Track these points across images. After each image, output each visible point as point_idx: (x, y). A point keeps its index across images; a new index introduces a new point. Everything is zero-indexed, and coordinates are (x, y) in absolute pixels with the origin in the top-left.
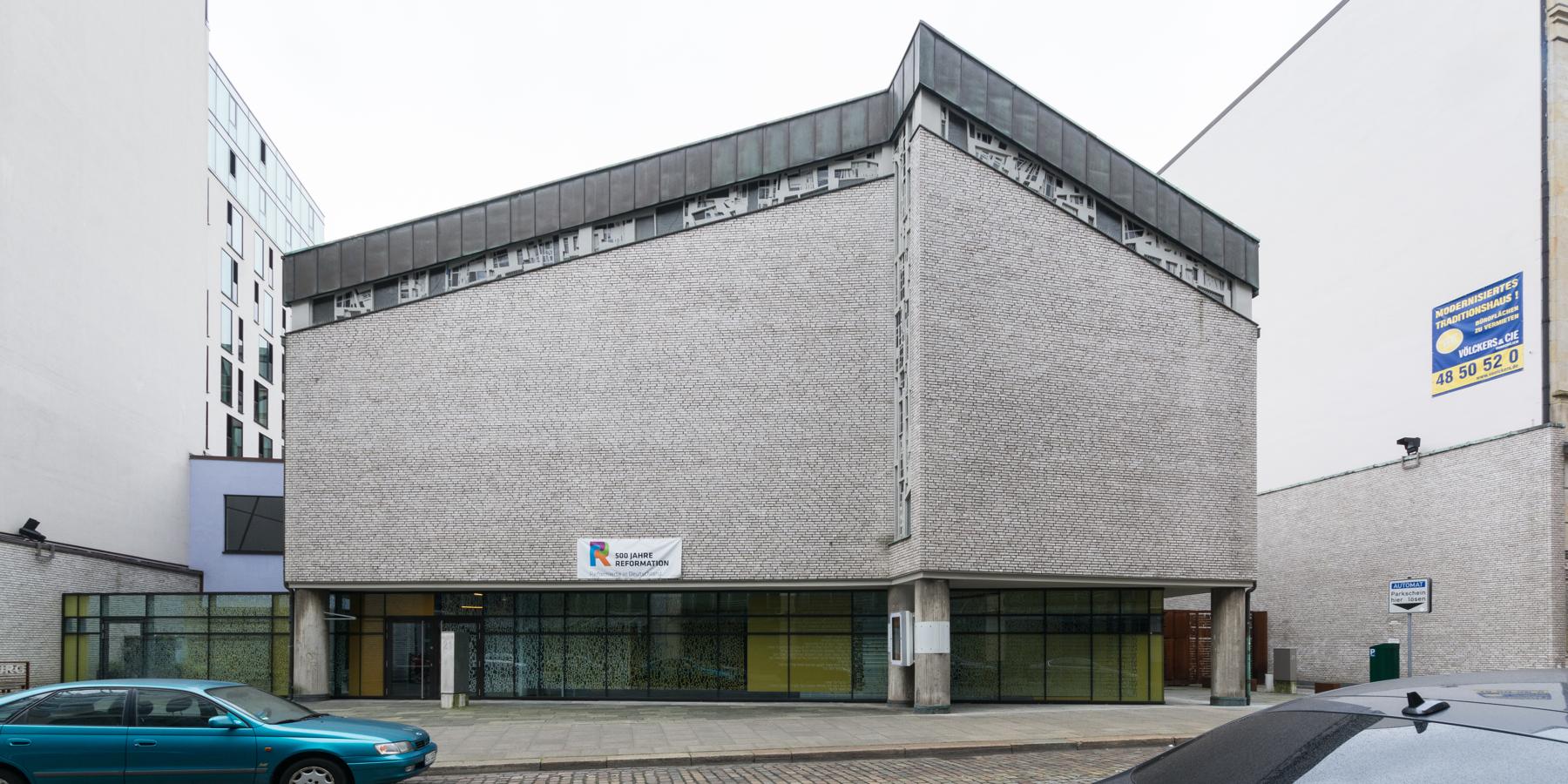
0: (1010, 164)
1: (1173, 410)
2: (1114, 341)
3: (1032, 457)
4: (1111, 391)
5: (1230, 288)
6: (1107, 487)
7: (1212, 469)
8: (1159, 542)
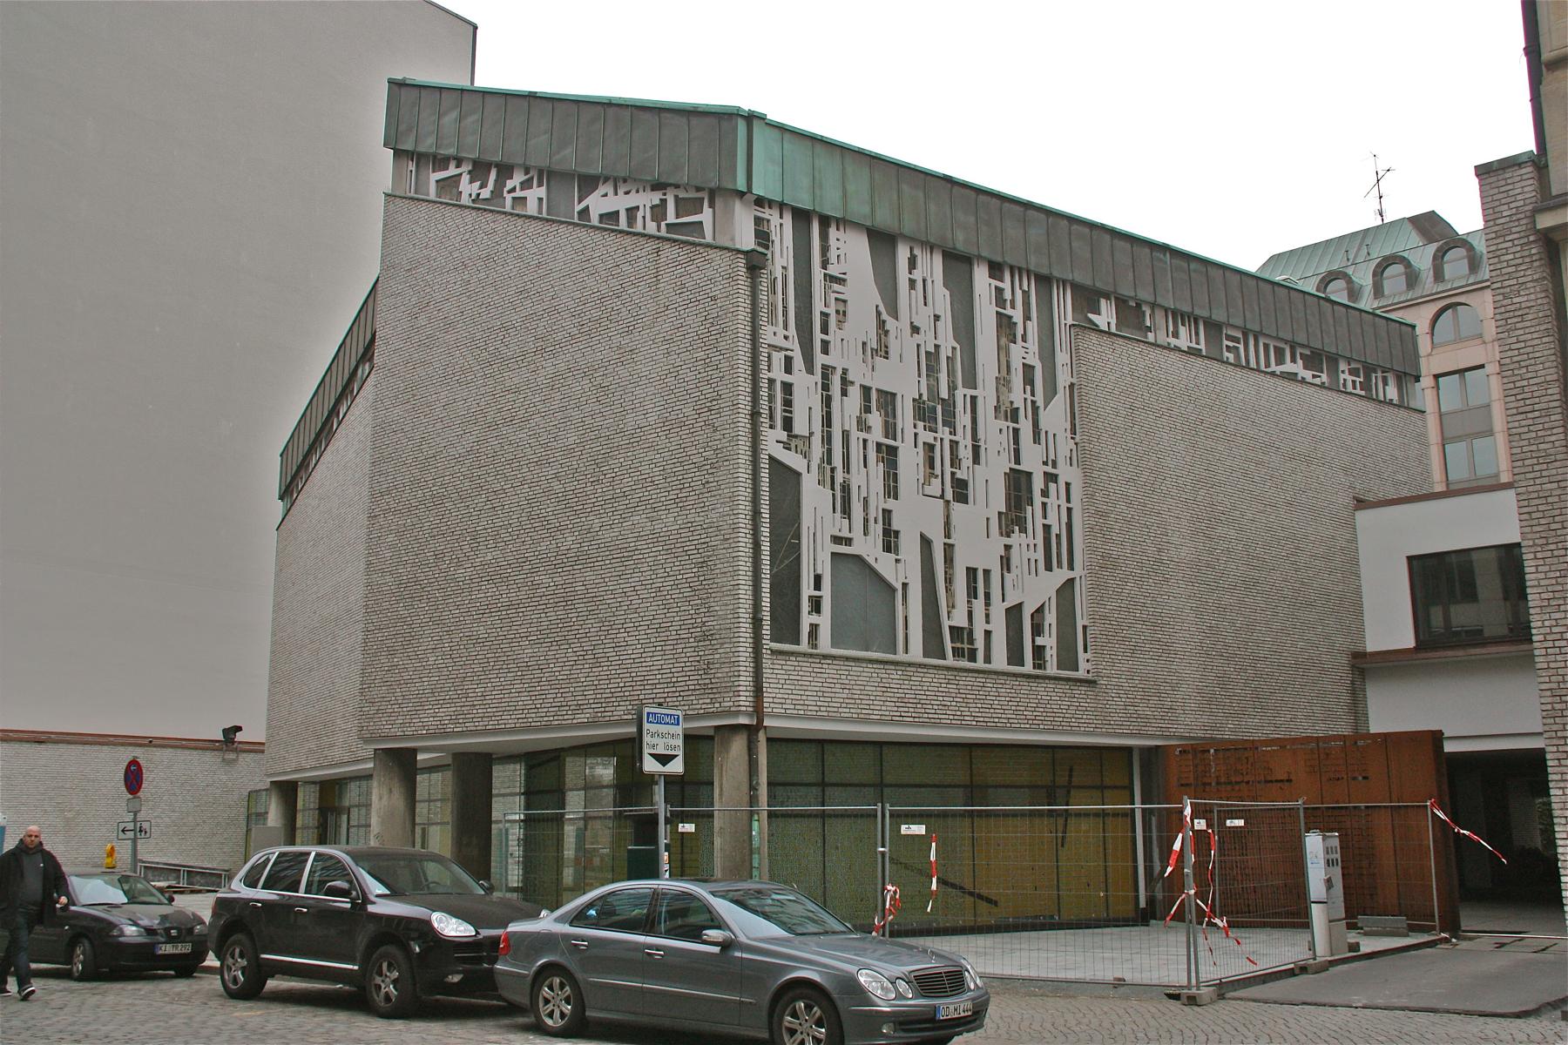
3: (459, 565)
7: (670, 521)
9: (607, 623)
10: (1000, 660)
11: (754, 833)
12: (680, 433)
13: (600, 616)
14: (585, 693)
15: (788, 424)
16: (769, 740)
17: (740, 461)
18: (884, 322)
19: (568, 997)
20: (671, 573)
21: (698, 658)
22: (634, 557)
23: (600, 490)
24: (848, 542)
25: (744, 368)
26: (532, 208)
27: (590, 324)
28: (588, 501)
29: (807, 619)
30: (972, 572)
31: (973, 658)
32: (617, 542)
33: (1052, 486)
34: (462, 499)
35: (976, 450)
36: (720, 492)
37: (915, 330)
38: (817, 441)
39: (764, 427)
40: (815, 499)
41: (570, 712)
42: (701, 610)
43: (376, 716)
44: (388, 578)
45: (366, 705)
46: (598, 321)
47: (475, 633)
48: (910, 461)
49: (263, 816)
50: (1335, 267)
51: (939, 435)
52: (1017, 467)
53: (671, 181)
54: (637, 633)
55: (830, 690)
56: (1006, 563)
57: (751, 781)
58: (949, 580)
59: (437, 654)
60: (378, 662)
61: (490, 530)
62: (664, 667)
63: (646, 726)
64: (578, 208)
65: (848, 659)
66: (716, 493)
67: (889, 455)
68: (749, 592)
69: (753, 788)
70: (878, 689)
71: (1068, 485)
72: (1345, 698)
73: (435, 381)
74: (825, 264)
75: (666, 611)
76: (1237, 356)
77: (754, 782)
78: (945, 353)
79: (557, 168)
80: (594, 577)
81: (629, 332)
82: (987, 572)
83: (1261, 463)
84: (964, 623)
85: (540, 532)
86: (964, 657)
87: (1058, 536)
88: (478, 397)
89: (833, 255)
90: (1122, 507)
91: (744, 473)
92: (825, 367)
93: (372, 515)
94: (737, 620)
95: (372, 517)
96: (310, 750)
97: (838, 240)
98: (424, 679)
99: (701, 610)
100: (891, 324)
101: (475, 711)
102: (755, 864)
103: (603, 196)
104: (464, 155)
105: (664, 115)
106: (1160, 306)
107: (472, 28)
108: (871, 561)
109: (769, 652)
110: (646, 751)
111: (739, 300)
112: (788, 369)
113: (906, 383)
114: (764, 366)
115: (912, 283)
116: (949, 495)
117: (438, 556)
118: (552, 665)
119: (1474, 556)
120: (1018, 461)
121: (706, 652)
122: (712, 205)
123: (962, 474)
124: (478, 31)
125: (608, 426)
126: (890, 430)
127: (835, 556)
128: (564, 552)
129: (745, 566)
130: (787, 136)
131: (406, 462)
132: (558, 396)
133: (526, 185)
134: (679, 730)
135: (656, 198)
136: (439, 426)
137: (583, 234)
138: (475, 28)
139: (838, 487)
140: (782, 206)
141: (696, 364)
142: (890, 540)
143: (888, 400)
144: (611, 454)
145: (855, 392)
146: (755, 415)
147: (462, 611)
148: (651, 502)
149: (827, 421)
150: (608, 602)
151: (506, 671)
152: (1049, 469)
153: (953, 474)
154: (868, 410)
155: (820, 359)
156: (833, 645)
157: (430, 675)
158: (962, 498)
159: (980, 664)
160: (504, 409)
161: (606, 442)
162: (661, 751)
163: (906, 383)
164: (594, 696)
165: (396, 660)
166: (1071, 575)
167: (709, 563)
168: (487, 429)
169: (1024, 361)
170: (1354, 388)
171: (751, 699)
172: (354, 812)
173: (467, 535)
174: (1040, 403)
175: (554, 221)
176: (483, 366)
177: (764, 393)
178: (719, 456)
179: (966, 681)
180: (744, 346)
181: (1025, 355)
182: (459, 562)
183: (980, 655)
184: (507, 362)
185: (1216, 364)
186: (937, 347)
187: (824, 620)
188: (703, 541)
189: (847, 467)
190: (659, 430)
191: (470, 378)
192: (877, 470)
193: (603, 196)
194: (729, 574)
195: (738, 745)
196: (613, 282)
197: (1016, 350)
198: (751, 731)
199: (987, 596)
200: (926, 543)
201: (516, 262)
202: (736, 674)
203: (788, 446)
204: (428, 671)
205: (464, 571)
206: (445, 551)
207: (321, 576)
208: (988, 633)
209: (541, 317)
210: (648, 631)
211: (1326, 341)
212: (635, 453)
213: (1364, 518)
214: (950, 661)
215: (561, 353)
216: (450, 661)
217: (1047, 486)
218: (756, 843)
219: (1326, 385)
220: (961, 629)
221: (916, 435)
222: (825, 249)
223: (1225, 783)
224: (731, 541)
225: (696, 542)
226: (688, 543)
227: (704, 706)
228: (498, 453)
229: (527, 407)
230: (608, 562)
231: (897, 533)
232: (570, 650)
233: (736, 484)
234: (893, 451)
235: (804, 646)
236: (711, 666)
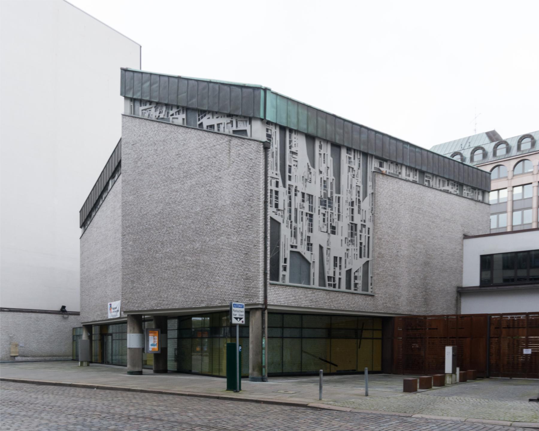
0: (154, 113)
1: (215, 210)
2: (188, 182)
3: (157, 252)
4: (187, 209)
5: (250, 123)
6: (185, 260)
7: (234, 239)
8: (208, 287)
9: (212, 274)
10: (343, 287)
11: (263, 343)
12: (239, 208)
13: (209, 271)
14: (204, 297)
15: (277, 206)
16: (268, 313)
17: (260, 218)
18: (310, 169)
20: (235, 257)
22: (222, 251)
23: (209, 228)
24: (296, 247)
25: (262, 185)
27: (204, 167)
28: (205, 231)
29: (282, 273)
31: (334, 286)
32: (216, 246)
33: (364, 229)
34: (157, 230)
35: (339, 216)
36: (253, 229)
39: (269, 207)
40: (285, 231)
41: (199, 303)
42: (246, 270)
43: (128, 304)
44: (130, 257)
45: (124, 300)
47: (163, 276)
48: (317, 219)
49: (80, 336)
50: (456, 150)
51: (327, 211)
52: (352, 222)
53: (235, 114)
54: (222, 277)
55: (288, 297)
56: (347, 255)
57: (262, 326)
59: (150, 283)
60: (128, 285)
61: (168, 241)
62: (233, 288)
63: (233, 308)
64: (198, 123)
65: (294, 287)
66: (251, 229)
68: (263, 264)
69: (263, 329)
70: (304, 297)
71: (369, 228)
72: (454, 302)
73: (145, 187)
74: (290, 147)
75: (233, 270)
77: (264, 327)
79: (190, 106)
80: (207, 258)
81: (219, 171)
82: (340, 258)
83: (433, 222)
85: (187, 242)
86: (331, 286)
87: (365, 246)
88: (162, 193)
89: (293, 144)
90: (386, 237)
91: (262, 223)
92: (289, 185)
93: (123, 234)
94: (259, 273)
95: (123, 235)
96: (98, 315)
97: (295, 138)
98: (145, 292)
99: (246, 270)
100: (312, 170)
102: (263, 353)
104: (153, 100)
105: (232, 87)
106: (404, 165)
108: (303, 254)
109: (269, 284)
110: (233, 316)
111: (261, 160)
112: (277, 186)
113: (316, 190)
114: (269, 185)
117: (149, 250)
118: (192, 287)
120: (353, 220)
121: (248, 284)
123: (334, 224)
124: (142, 48)
125: (212, 205)
126: (311, 208)
127: (291, 252)
128: (196, 249)
129: (262, 255)
130: (278, 97)
131: (136, 216)
132: (193, 194)
134: (243, 310)
136: (147, 203)
137: (201, 133)
139: (293, 228)
140: (276, 125)
141: (244, 183)
142: (310, 246)
143: (311, 196)
144: (213, 215)
145: (299, 195)
146: (266, 202)
147: (158, 268)
148: (228, 232)
149: (290, 205)
151: (175, 289)
152: (363, 223)
153: (331, 224)
154: (303, 201)
155: (288, 182)
156: (290, 281)
157: (147, 290)
158: (334, 233)
159: (337, 289)
160: (173, 198)
161: (211, 211)
162: (237, 316)
163: (316, 190)
165: (134, 285)
166: (368, 259)
167: (249, 254)
168: (166, 205)
169: (357, 184)
170: (468, 196)
171: (263, 299)
172: (114, 335)
173: (159, 242)
174: (361, 200)
175: (189, 128)
176: (163, 182)
177: (269, 194)
178: (253, 216)
179: (332, 295)
180: (262, 177)
181: (357, 182)
182: (157, 252)
183: (337, 286)
184: (172, 181)
185: (422, 187)
186: (327, 178)
187: (287, 273)
188: (247, 246)
189: (296, 222)
190: (230, 207)
191: (159, 186)
192: (306, 222)
194: (256, 258)
195: (258, 314)
196: (213, 152)
198: (263, 310)
199: (340, 266)
200: (321, 247)
201: (175, 143)
202: (258, 291)
203: (276, 213)
204: (147, 289)
205: (159, 255)
206: (151, 248)
207: (99, 255)
208: (340, 279)
209: (185, 164)
210: (227, 276)
211: (460, 178)
212: (222, 215)
213: (467, 242)
214: (327, 288)
215: (193, 178)
217: (362, 229)
218: (264, 346)
219: (458, 194)
220: (331, 277)
221: (319, 210)
222: (290, 142)
224: (257, 246)
225: (244, 246)
226: (241, 247)
227: (247, 302)
228: (170, 214)
229: (181, 197)
230: (212, 253)
231: (311, 245)
232: (198, 282)
233: (259, 227)
234: (311, 216)
235: (280, 282)
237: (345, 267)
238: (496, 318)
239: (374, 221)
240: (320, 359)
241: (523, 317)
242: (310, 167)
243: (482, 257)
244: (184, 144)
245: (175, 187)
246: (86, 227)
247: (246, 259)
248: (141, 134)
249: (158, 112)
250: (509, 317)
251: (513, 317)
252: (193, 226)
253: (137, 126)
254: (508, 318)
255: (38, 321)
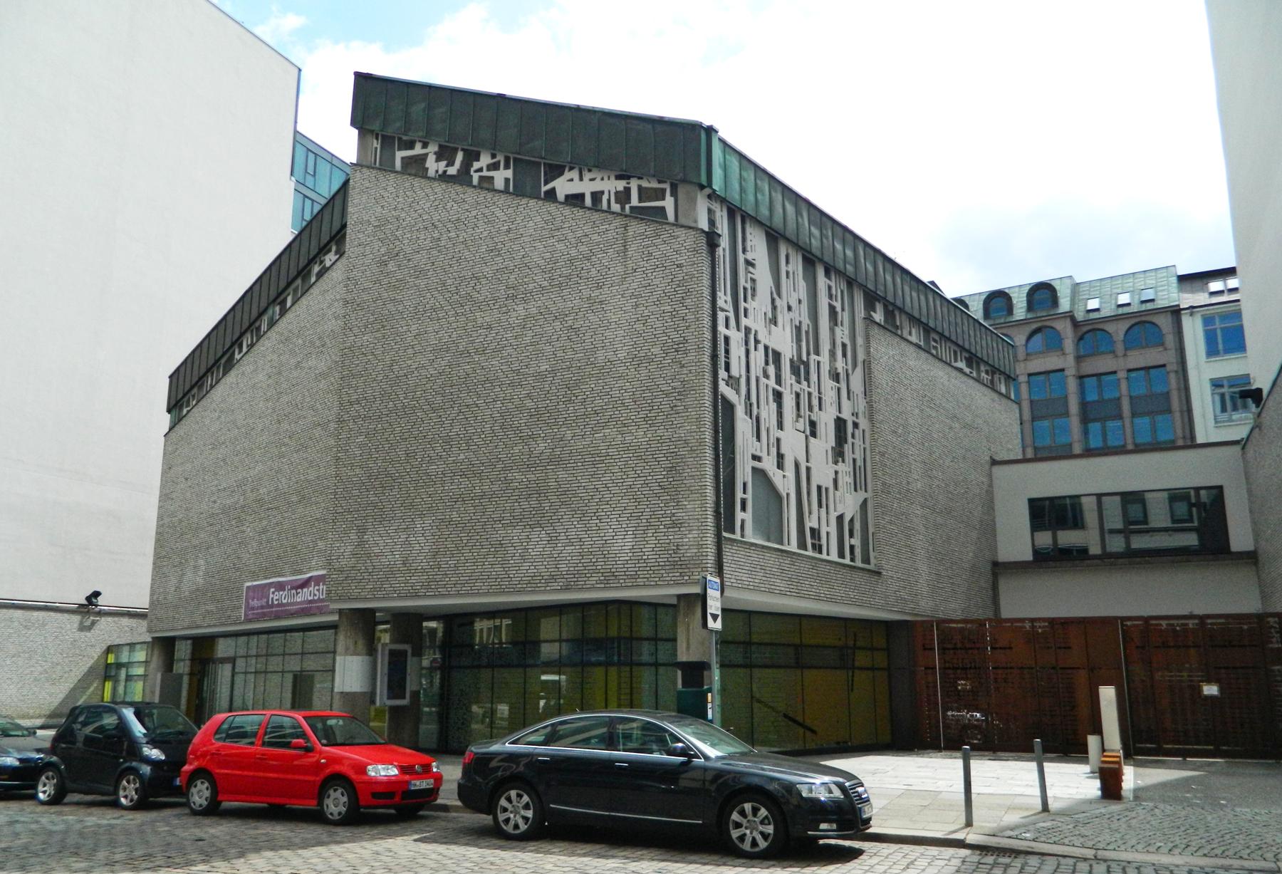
4: (515, 366)
7: (640, 436)
19: (527, 804)
21: (668, 541)
26: (499, 184)
29: (739, 515)
30: (819, 488)
36: (687, 414)
37: (789, 308)
38: (743, 381)
40: (743, 426)
41: (543, 581)
46: (569, 277)
48: (789, 401)
58: (809, 493)
64: (544, 189)
67: (778, 396)
71: (864, 431)
74: (744, 251)
76: (937, 352)
78: (804, 328)
82: (827, 489)
84: (816, 526)
89: (749, 244)
100: (778, 302)
101: (448, 579)
103: (568, 181)
107: (297, 71)
115: (788, 273)
116: (808, 432)
119: (1148, 496)
121: (676, 537)
122: (674, 193)
124: (302, 73)
133: (494, 167)
135: (621, 185)
136: (410, 351)
138: (300, 70)
145: (761, 347)
150: (580, 495)
153: (809, 416)
158: (814, 434)
159: (824, 556)
164: (567, 569)
166: (866, 495)
167: (678, 468)
174: (850, 372)
186: (800, 322)
193: (568, 181)
196: (583, 248)
197: (838, 330)
200: (797, 466)
202: (704, 554)
216: (423, 538)
223: (961, 649)
233: (702, 409)
236: (681, 548)
237: (835, 511)
238: (1134, 626)
239: (871, 419)
240: (785, 716)
241: (1193, 624)
242: (775, 296)
243: (1032, 502)
244: (509, 231)
245: (483, 317)
246: (185, 411)
247: (671, 479)
248: (400, 206)
249: (444, 163)
250: (1164, 623)
251: (1173, 625)
252: (529, 403)
253: (391, 189)
254: (1161, 625)
255: (29, 629)
